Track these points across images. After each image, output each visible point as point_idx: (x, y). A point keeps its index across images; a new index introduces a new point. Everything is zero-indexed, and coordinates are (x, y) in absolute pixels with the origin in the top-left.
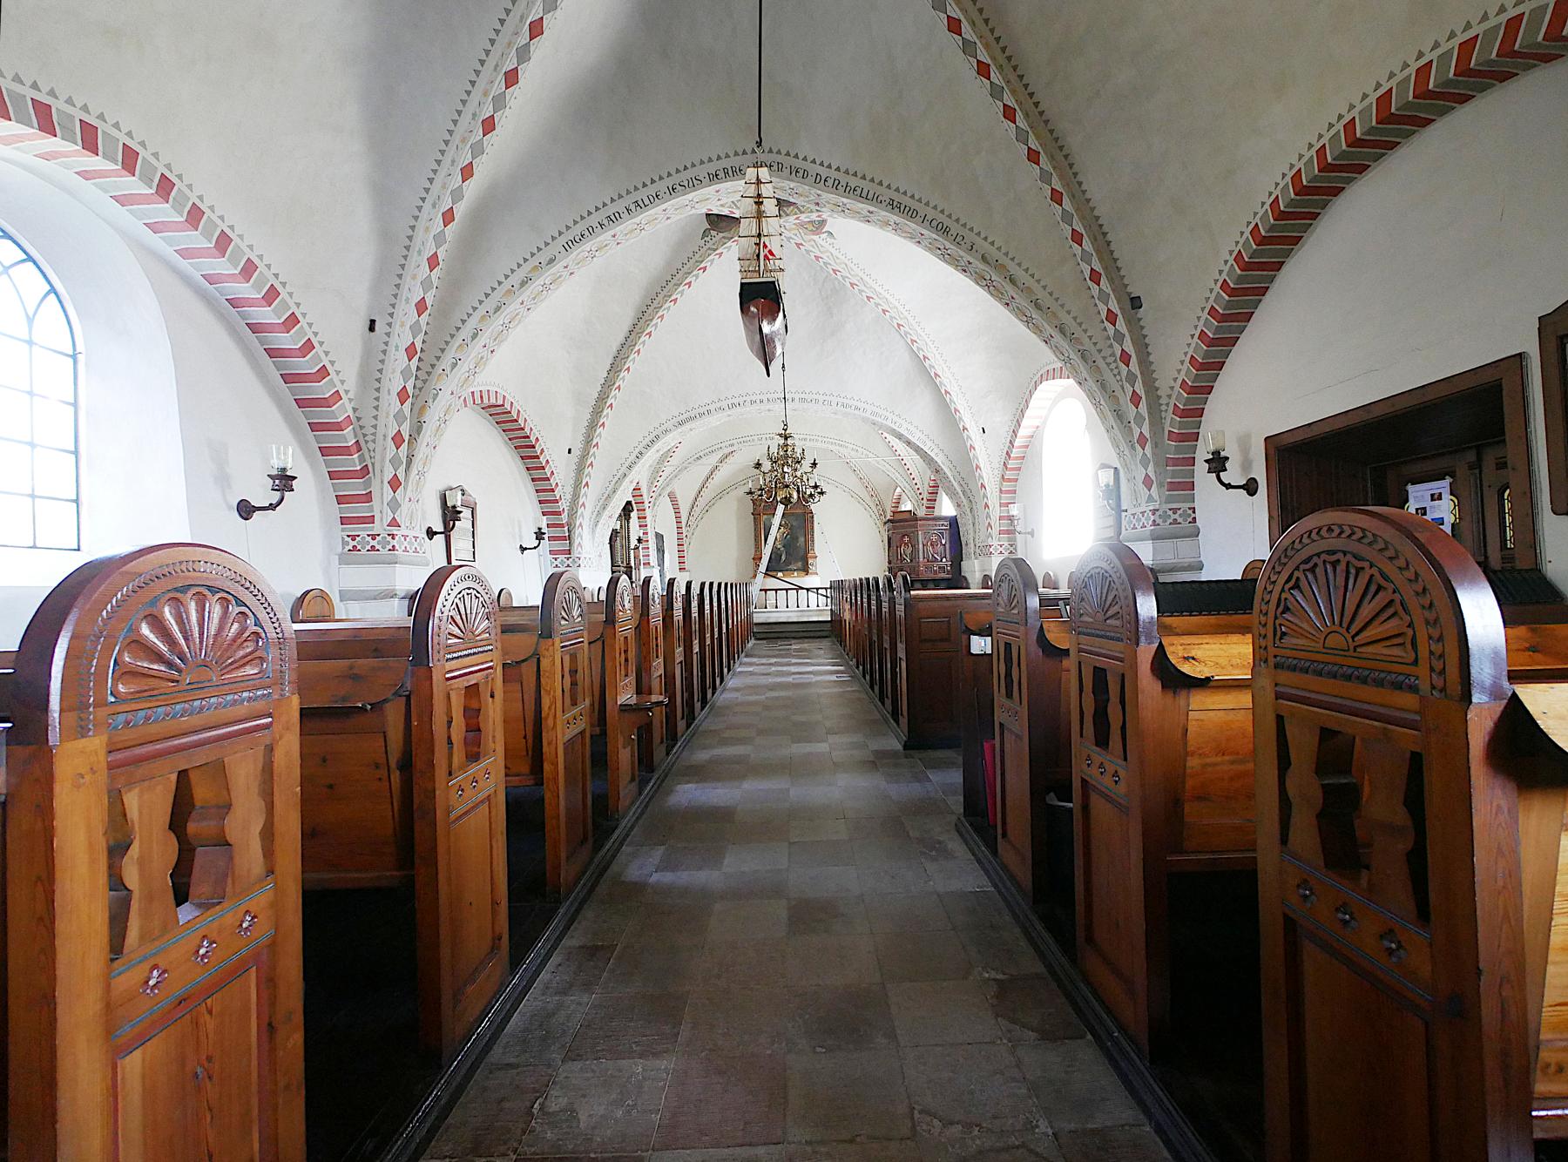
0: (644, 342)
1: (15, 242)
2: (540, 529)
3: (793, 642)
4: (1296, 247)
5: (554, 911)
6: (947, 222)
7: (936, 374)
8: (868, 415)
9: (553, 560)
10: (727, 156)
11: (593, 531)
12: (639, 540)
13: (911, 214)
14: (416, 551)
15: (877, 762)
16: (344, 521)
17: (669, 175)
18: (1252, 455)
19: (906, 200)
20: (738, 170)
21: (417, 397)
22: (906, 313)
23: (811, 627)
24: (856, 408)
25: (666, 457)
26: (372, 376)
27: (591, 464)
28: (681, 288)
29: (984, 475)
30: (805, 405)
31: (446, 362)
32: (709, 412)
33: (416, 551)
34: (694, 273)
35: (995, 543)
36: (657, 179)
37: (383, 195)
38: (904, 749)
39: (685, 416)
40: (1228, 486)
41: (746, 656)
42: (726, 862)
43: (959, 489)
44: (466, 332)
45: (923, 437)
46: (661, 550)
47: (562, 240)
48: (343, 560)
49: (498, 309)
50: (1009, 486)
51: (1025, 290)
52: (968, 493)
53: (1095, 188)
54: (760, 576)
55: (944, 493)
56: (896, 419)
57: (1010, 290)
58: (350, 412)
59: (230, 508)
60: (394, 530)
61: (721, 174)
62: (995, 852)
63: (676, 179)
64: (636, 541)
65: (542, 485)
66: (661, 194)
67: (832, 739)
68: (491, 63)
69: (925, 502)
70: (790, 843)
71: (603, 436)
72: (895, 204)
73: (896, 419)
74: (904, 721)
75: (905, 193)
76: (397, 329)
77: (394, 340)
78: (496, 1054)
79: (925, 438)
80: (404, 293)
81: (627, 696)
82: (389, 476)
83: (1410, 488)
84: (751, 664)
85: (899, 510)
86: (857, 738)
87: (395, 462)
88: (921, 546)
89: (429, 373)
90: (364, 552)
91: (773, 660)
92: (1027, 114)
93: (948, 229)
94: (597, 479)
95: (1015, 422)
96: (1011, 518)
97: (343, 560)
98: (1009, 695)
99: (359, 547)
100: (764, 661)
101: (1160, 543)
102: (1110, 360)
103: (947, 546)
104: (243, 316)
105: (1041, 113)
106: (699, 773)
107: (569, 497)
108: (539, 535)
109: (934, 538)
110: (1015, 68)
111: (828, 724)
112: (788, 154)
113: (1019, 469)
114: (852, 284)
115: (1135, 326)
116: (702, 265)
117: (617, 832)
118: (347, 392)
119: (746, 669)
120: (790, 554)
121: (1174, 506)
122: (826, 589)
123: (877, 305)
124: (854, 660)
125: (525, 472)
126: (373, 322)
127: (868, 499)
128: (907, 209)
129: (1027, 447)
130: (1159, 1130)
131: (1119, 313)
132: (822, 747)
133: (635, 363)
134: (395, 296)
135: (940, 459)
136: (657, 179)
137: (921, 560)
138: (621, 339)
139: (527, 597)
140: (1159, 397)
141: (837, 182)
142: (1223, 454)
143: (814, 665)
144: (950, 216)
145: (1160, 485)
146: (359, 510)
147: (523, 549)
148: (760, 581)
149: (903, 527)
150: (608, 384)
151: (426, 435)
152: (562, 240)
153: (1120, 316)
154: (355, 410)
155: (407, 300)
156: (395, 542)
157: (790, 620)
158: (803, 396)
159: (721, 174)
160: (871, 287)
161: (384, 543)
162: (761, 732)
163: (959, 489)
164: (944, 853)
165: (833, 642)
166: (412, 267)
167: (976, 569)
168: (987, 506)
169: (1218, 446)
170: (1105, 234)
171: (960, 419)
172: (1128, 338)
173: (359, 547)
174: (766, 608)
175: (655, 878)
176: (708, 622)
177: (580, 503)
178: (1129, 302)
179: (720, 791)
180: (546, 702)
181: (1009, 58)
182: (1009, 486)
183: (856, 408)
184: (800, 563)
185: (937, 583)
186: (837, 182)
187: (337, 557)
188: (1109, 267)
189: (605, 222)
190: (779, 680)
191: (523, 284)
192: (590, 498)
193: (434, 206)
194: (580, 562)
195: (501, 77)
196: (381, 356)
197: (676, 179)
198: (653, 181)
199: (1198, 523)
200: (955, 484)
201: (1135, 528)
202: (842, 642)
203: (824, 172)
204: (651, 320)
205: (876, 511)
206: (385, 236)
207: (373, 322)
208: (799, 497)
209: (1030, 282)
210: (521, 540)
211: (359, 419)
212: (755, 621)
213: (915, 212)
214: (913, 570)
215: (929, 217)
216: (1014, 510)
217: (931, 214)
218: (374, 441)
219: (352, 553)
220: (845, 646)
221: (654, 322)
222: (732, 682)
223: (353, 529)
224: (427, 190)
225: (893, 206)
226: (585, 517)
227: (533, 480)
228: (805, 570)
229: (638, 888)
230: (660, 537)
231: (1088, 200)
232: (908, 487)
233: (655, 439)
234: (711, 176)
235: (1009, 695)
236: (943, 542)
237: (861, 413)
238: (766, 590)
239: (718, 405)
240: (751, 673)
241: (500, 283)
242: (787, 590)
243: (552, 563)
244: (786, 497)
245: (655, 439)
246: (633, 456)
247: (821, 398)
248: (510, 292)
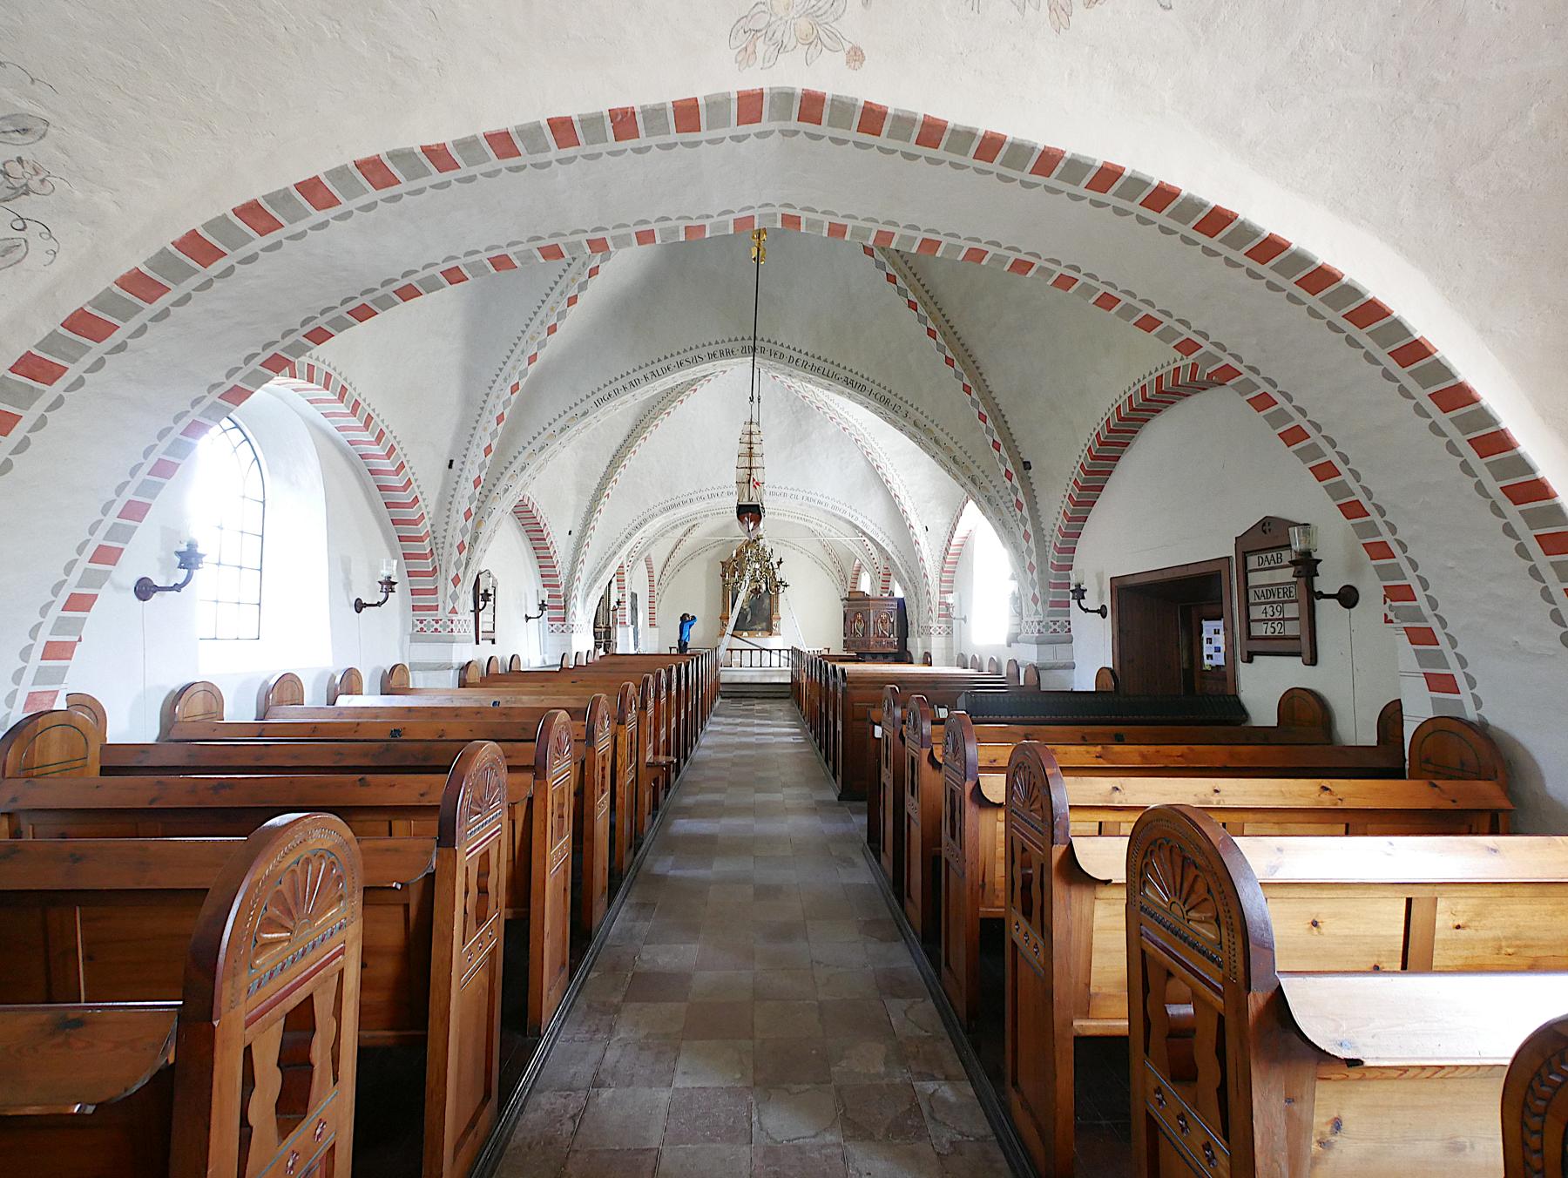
0: (640, 445)
1: (242, 431)
2: (543, 601)
3: (756, 701)
4: (1127, 448)
5: (620, 886)
6: (888, 396)
7: (887, 481)
8: (829, 509)
10: (723, 342)
11: (585, 601)
12: (618, 603)
13: (861, 388)
14: (465, 632)
15: (819, 808)
16: (414, 608)
18: (1104, 588)
19: (857, 379)
21: (477, 516)
22: (863, 431)
23: (771, 689)
24: (819, 502)
26: (446, 502)
27: (588, 544)
28: (674, 404)
29: (927, 566)
30: (775, 498)
31: (500, 488)
32: (691, 500)
33: (465, 632)
34: (687, 393)
35: (934, 625)
36: (669, 356)
37: (469, 375)
38: (839, 800)
39: (670, 503)
40: (1086, 610)
41: (714, 715)
42: (714, 866)
43: (905, 576)
44: (516, 465)
46: (634, 609)
47: (594, 398)
48: (413, 639)
49: (542, 448)
50: (948, 577)
51: (946, 449)
52: (915, 580)
53: (996, 383)
54: (727, 637)
55: (896, 582)
56: (852, 513)
57: (935, 448)
58: (429, 528)
59: (351, 605)
60: (455, 617)
61: (718, 354)
62: (879, 862)
63: (682, 357)
64: (615, 604)
65: (542, 553)
66: (672, 367)
67: (786, 791)
68: (558, 290)
69: (881, 575)
70: (755, 857)
71: (600, 521)
73: (852, 513)
74: (839, 778)
76: (468, 465)
77: (465, 474)
78: (608, 942)
79: (878, 531)
80: (476, 441)
81: (649, 757)
82: (452, 575)
83: (1204, 623)
84: (719, 724)
85: (857, 590)
86: (806, 790)
87: (457, 565)
88: (872, 623)
89: (486, 496)
90: (429, 632)
91: (739, 720)
92: (945, 333)
94: (590, 557)
95: (949, 533)
96: (948, 606)
97: (413, 639)
98: (887, 767)
99: (425, 629)
100: (730, 720)
101: (1044, 647)
102: (1008, 504)
103: (895, 624)
104: (367, 465)
105: (955, 333)
106: (687, 812)
107: (566, 571)
108: (542, 606)
109: (884, 616)
110: (936, 303)
111: (783, 779)
112: (769, 341)
113: (956, 563)
114: (818, 408)
115: (1027, 484)
116: (694, 388)
117: (644, 846)
118: (428, 513)
119: (716, 729)
120: (756, 615)
121: (1053, 619)
122: (788, 650)
123: (838, 424)
124: (809, 724)
125: (531, 550)
126: (451, 461)
127: (830, 565)
128: (858, 385)
129: (963, 545)
130: (919, 967)
131: (1014, 472)
132: (778, 797)
133: (631, 461)
134: (469, 442)
135: (889, 549)
136: (669, 356)
137: (872, 635)
138: (620, 441)
139: (529, 660)
140: (1044, 536)
142: (1082, 587)
143: (774, 727)
144: (890, 392)
145: (1044, 602)
146: (426, 600)
147: (528, 618)
148: (727, 641)
149: (857, 605)
150: (607, 478)
151: (481, 544)
152: (594, 398)
153: (1014, 474)
154: (432, 525)
155: (478, 445)
156: (453, 626)
157: (753, 681)
158: (773, 490)
159: (718, 354)
160: (834, 410)
161: (445, 626)
162: (732, 784)
163: (905, 576)
164: (853, 865)
165: (792, 703)
166: (484, 421)
167: (919, 646)
168: (928, 593)
169: (1080, 581)
170: (1003, 416)
171: (907, 518)
172: (1020, 491)
173: (425, 629)
174: (731, 666)
175: (671, 873)
176: (690, 688)
177: (576, 578)
178: (1022, 465)
179: (705, 825)
180: (619, 762)
181: (931, 297)
182: (948, 577)
183: (819, 502)
184: (764, 624)
185: (885, 657)
187: (409, 637)
188: (1006, 440)
189: (628, 386)
190: (744, 739)
191: (562, 430)
192: (584, 573)
193: (505, 380)
195: (566, 300)
196: (455, 485)
197: (682, 357)
198: (666, 358)
199: (1072, 633)
200: (903, 572)
201: (1027, 633)
202: (799, 704)
203: (796, 355)
204: (648, 427)
205: (837, 576)
206: (467, 400)
207: (451, 461)
208: (767, 588)
209: (950, 444)
210: (526, 610)
211: (434, 532)
212: (721, 681)
214: (866, 643)
216: (950, 599)
217: (876, 389)
218: (442, 548)
219: (419, 634)
220: (802, 710)
221: (650, 429)
222: (704, 740)
223: (421, 614)
224: (501, 370)
225: (848, 382)
226: (579, 589)
227: (538, 558)
228: (769, 630)
229: (660, 879)
230: (634, 596)
231: (991, 392)
232: (865, 559)
235: (887, 767)
237: (822, 506)
238: (731, 650)
239: (700, 495)
240: (722, 733)
241: (544, 429)
242: (751, 650)
243: (549, 628)
244: (756, 589)
246: (623, 537)
247: (789, 492)
248: (553, 436)
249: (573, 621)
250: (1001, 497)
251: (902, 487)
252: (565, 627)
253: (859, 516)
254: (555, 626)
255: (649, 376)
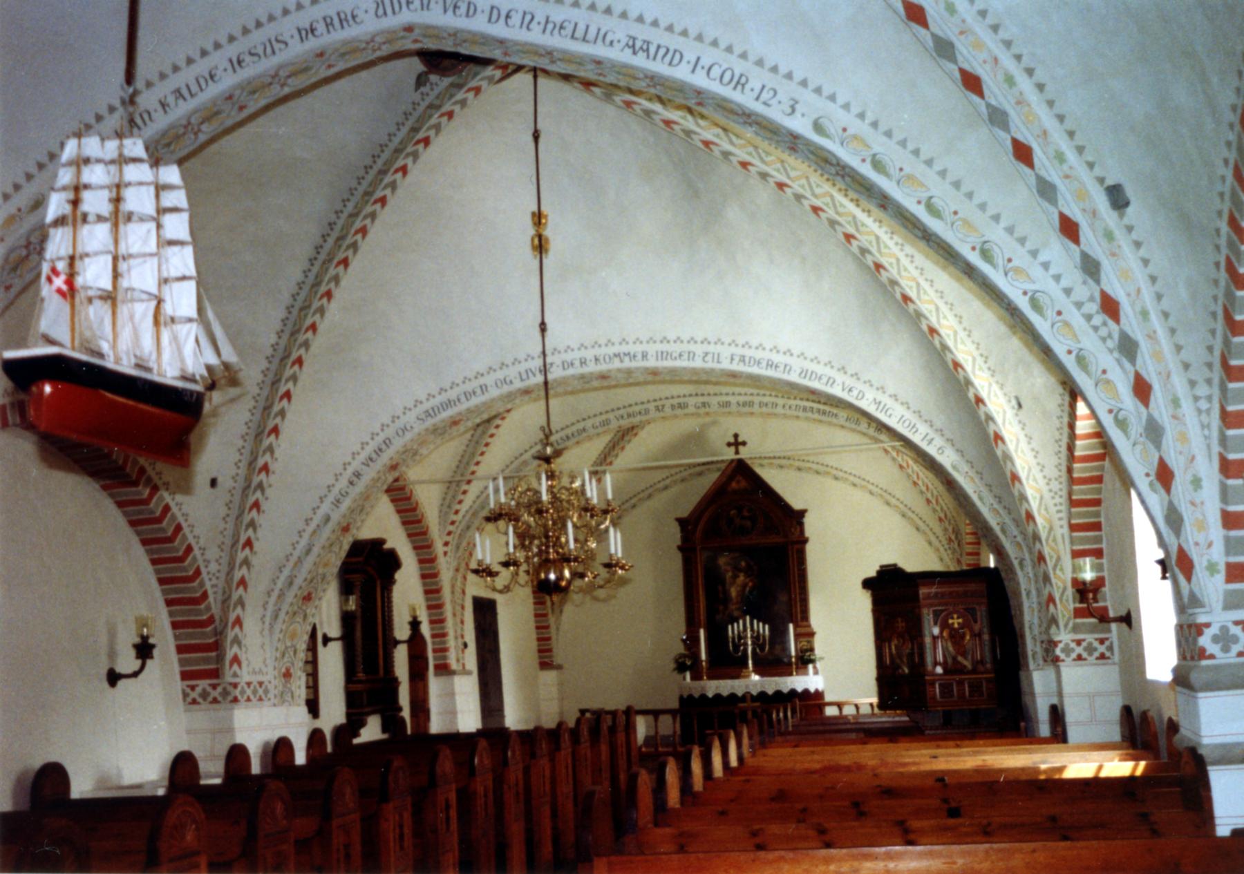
6: (739, 67)
9: (188, 690)
17: (232, 39)
20: (349, 18)
25: (473, 455)
45: (908, 415)
72: (638, 44)
73: (850, 382)
75: (655, 23)
79: (914, 419)
93: (743, 80)
128: (662, 52)
135: (947, 458)
141: (528, 18)
158: (665, 347)
186: (528, 18)
194: (237, 692)
213: (677, 56)
215: (706, 62)
233: (384, 447)
234: (304, 33)
236: (977, 628)
243: (1110, 648)
245: (384, 447)
249: (235, 675)
250: (1068, 291)
251: (944, 309)
252: (219, 689)
253: (865, 388)
254: (199, 690)
255: (171, 100)
